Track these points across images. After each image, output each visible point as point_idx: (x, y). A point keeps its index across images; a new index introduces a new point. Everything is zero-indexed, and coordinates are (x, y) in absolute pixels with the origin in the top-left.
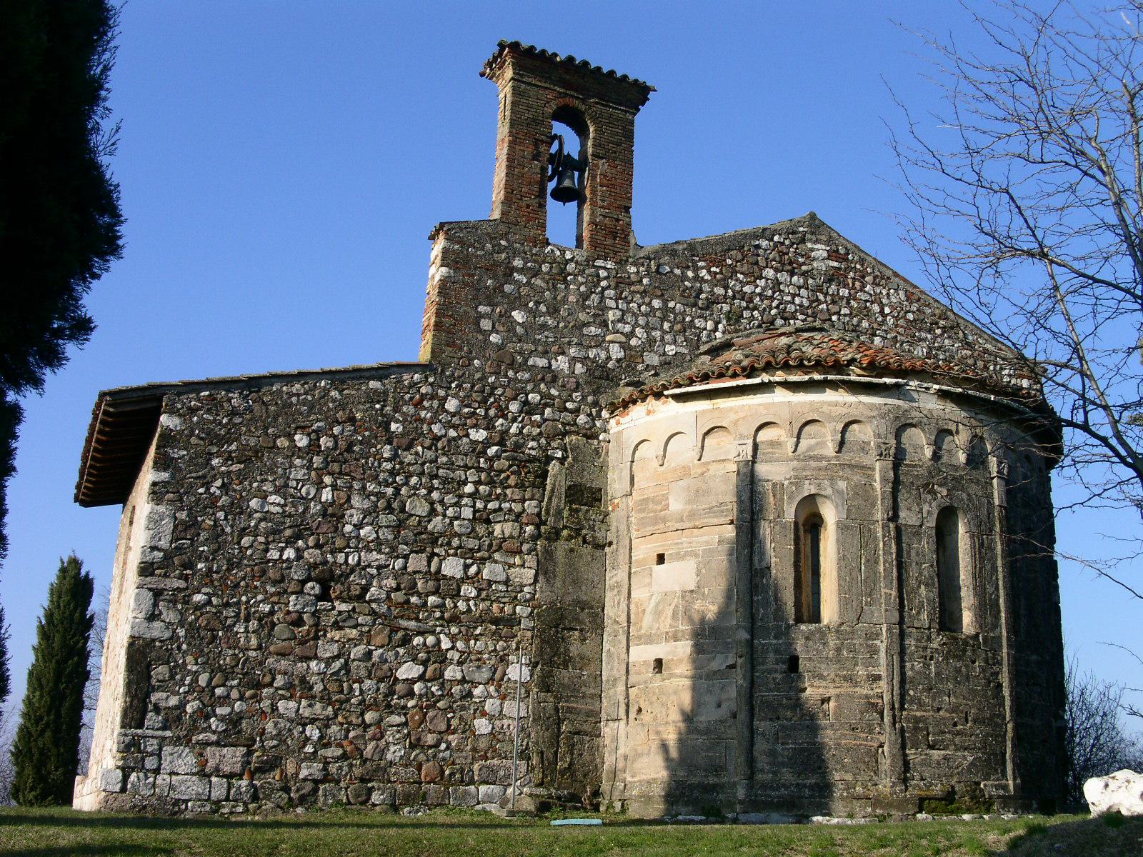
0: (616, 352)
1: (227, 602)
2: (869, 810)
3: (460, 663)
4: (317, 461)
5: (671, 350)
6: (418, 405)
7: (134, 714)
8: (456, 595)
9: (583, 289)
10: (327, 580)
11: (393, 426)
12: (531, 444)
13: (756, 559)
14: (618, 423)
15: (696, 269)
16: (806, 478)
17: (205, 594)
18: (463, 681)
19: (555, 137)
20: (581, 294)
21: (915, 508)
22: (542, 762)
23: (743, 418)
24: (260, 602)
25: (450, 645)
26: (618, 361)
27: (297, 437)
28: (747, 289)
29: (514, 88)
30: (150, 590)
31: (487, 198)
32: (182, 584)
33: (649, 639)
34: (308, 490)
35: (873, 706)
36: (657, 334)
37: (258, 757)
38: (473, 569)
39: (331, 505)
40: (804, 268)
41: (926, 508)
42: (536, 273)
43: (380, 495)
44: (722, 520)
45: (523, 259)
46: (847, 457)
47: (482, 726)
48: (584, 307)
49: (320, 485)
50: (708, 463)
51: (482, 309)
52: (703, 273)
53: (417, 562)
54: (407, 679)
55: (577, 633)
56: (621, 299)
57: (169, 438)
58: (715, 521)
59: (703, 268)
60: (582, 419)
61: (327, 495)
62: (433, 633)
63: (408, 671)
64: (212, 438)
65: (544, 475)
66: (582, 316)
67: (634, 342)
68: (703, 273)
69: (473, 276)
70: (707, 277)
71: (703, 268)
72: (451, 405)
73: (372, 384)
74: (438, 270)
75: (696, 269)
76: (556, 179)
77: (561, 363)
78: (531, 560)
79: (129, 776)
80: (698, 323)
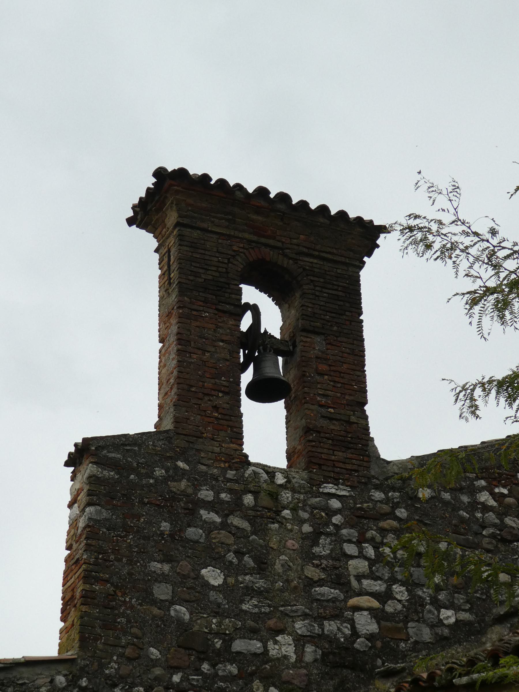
0: (366, 624)
5: (448, 616)
9: (307, 528)
15: (473, 491)
19: (248, 307)
20: (305, 537)
26: (371, 637)
29: (181, 237)
31: (134, 406)
36: (424, 593)
45: (212, 488)
51: (156, 566)
52: (484, 497)
56: (366, 541)
59: (483, 489)
66: (311, 572)
67: (389, 608)
69: (138, 517)
70: (492, 503)
71: (483, 489)
74: (83, 511)
76: (251, 367)
77: (284, 647)
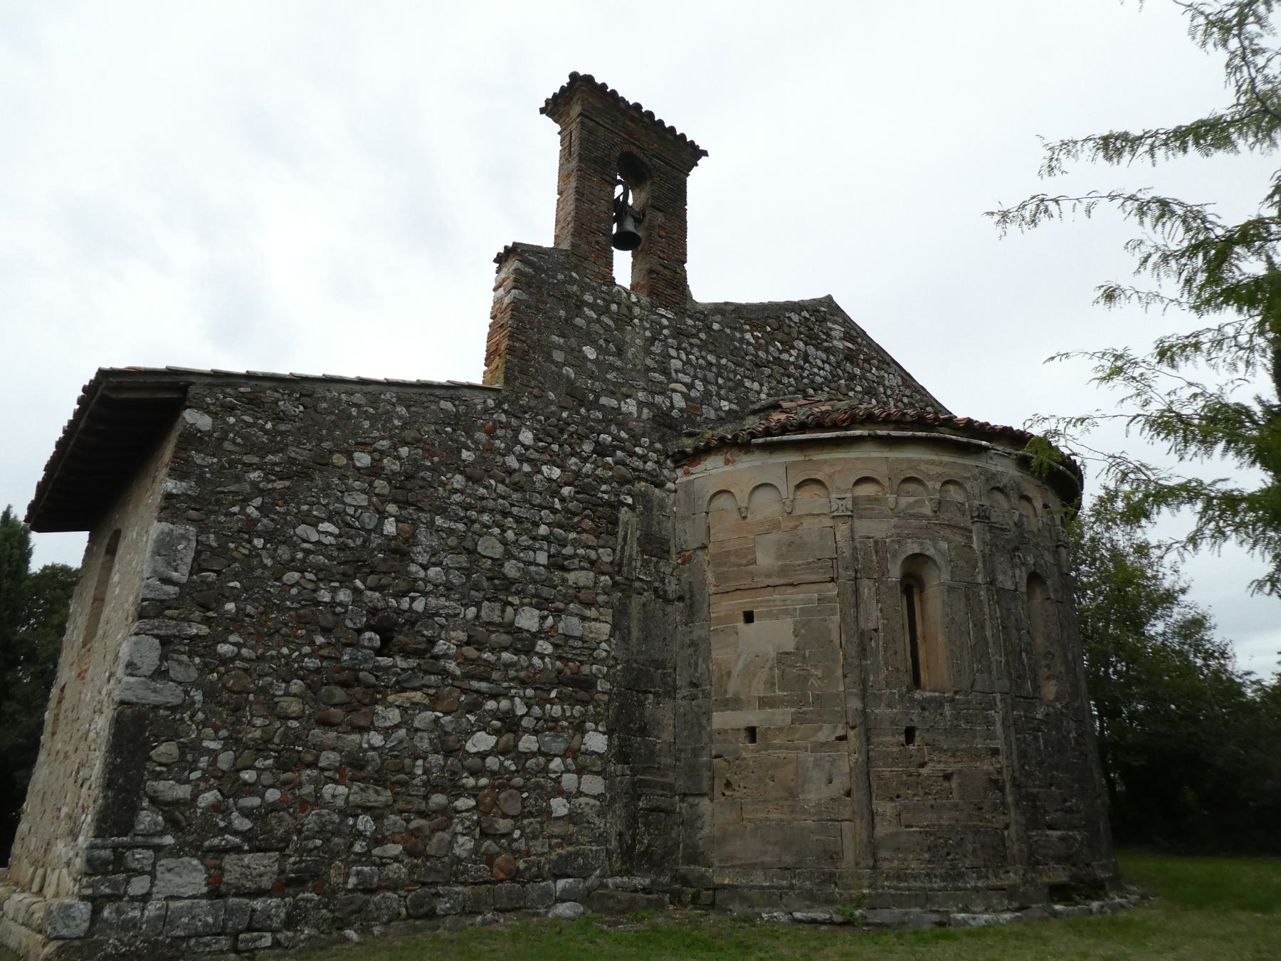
0: (679, 401)
1: (263, 654)
2: (1006, 902)
3: (535, 732)
4: (381, 485)
5: (725, 405)
6: (491, 433)
7: (115, 817)
8: (529, 651)
10: (388, 630)
11: (465, 454)
12: (604, 487)
13: (861, 620)
14: (687, 473)
16: (908, 536)
17: (234, 644)
18: (540, 752)
20: (647, 339)
21: (1010, 572)
22: (621, 847)
23: (839, 472)
24: (306, 655)
25: (524, 710)
27: (356, 455)
28: (785, 356)
30: (156, 636)
32: (204, 630)
33: (734, 703)
34: (370, 520)
35: (997, 785)
36: (713, 388)
37: (294, 863)
38: (550, 621)
39: (395, 538)
40: (826, 344)
41: (1017, 572)
42: (606, 310)
43: (451, 532)
44: (819, 577)
46: (945, 517)
47: (559, 806)
48: (649, 353)
49: (383, 515)
50: (800, 516)
52: (748, 336)
53: (490, 612)
54: (478, 753)
55: (651, 696)
57: (192, 438)
58: (813, 578)
60: (650, 466)
61: (390, 527)
62: (505, 696)
63: (482, 742)
64: (250, 447)
65: (615, 522)
67: (693, 394)
68: (748, 336)
72: (527, 437)
73: (443, 404)
75: (743, 331)
78: (608, 614)
79: (102, 909)
80: (748, 383)
